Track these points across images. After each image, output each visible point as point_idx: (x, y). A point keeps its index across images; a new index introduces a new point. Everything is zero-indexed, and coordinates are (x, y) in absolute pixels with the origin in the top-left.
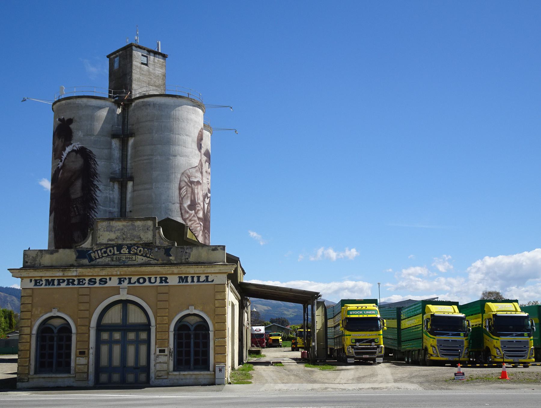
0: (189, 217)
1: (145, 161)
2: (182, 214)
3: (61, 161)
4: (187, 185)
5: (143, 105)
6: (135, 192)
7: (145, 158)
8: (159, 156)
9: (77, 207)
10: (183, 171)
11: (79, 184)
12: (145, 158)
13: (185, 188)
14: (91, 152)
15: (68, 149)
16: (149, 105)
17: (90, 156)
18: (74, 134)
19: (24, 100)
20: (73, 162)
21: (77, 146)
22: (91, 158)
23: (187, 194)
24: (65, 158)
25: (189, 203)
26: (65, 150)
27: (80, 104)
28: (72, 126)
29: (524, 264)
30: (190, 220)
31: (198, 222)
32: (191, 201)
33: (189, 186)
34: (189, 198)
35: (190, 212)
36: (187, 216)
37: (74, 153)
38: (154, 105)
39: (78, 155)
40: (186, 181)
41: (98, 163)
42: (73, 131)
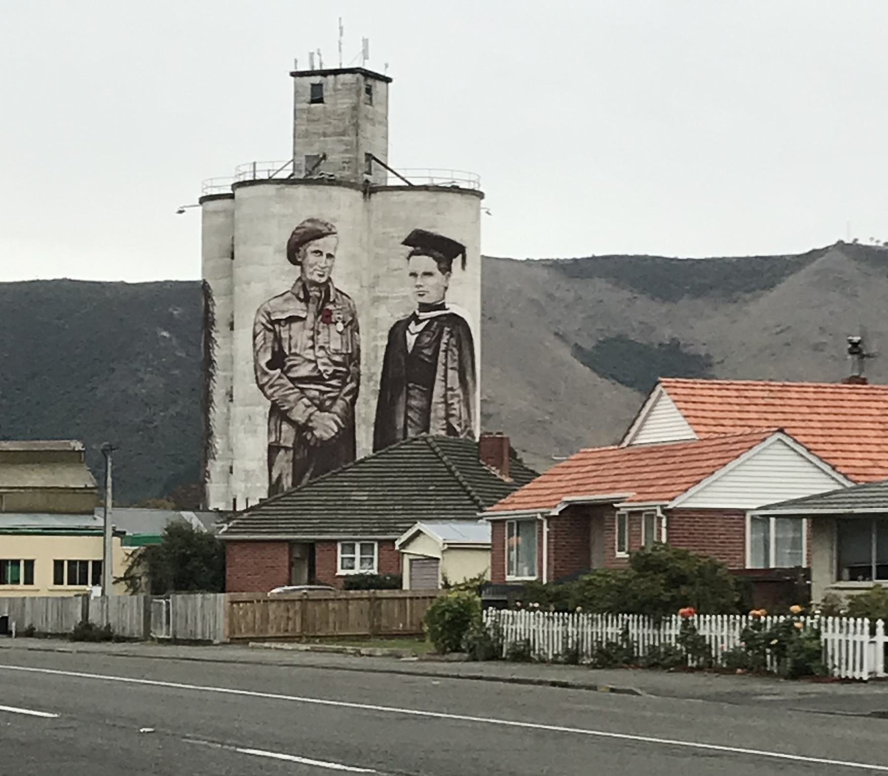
0: (270, 380)
2: (257, 378)
4: (266, 328)
10: (258, 307)
13: (262, 334)
19: (181, 212)
23: (265, 343)
25: (269, 357)
29: (37, 630)
30: (272, 386)
31: (291, 385)
32: (274, 353)
33: (270, 330)
34: (270, 350)
35: (272, 372)
36: (266, 379)
40: (264, 321)
41: (216, 302)
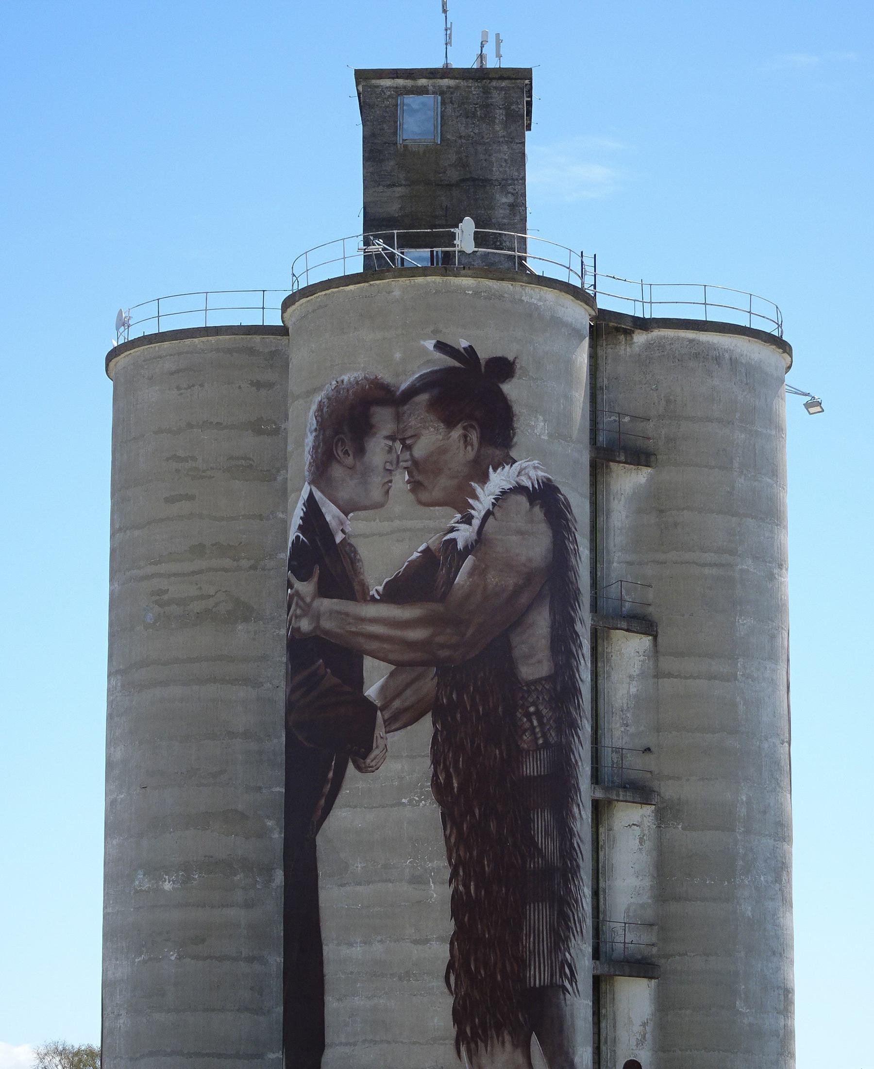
1: (706, 571)
3: (468, 520)
5: (696, 356)
6: (667, 684)
7: (709, 557)
8: (750, 561)
9: (538, 713)
11: (541, 623)
12: (709, 557)
14: (568, 506)
15: (500, 479)
16: (718, 360)
17: (567, 520)
18: (519, 424)
20: (520, 533)
21: (533, 474)
22: (569, 530)
24: (489, 514)
26: (484, 479)
27: (537, 308)
28: (508, 388)
37: (523, 500)
38: (734, 362)
39: (537, 509)
42: (516, 409)
